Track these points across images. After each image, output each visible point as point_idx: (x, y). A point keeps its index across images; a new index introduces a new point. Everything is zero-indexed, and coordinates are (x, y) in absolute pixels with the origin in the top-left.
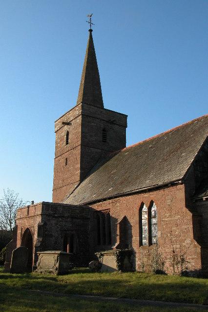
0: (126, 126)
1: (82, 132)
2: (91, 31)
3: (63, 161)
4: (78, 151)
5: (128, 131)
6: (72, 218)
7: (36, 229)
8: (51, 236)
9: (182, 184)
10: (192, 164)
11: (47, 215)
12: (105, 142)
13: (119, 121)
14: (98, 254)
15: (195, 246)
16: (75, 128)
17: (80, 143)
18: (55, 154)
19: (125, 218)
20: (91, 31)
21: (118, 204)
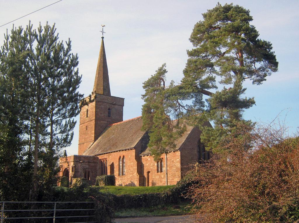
0: (123, 105)
1: (96, 112)
2: (103, 38)
3: (84, 127)
4: (93, 123)
5: (125, 109)
6: (89, 162)
7: (71, 168)
8: (78, 172)
9: (134, 149)
10: (140, 140)
11: (76, 161)
12: (110, 116)
13: (119, 102)
14: (24, 120)
15: (137, 176)
16: (92, 109)
17: (94, 118)
18: (80, 123)
19: (113, 163)
20: (103, 38)
21: (110, 156)
